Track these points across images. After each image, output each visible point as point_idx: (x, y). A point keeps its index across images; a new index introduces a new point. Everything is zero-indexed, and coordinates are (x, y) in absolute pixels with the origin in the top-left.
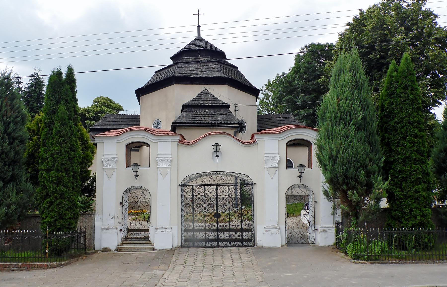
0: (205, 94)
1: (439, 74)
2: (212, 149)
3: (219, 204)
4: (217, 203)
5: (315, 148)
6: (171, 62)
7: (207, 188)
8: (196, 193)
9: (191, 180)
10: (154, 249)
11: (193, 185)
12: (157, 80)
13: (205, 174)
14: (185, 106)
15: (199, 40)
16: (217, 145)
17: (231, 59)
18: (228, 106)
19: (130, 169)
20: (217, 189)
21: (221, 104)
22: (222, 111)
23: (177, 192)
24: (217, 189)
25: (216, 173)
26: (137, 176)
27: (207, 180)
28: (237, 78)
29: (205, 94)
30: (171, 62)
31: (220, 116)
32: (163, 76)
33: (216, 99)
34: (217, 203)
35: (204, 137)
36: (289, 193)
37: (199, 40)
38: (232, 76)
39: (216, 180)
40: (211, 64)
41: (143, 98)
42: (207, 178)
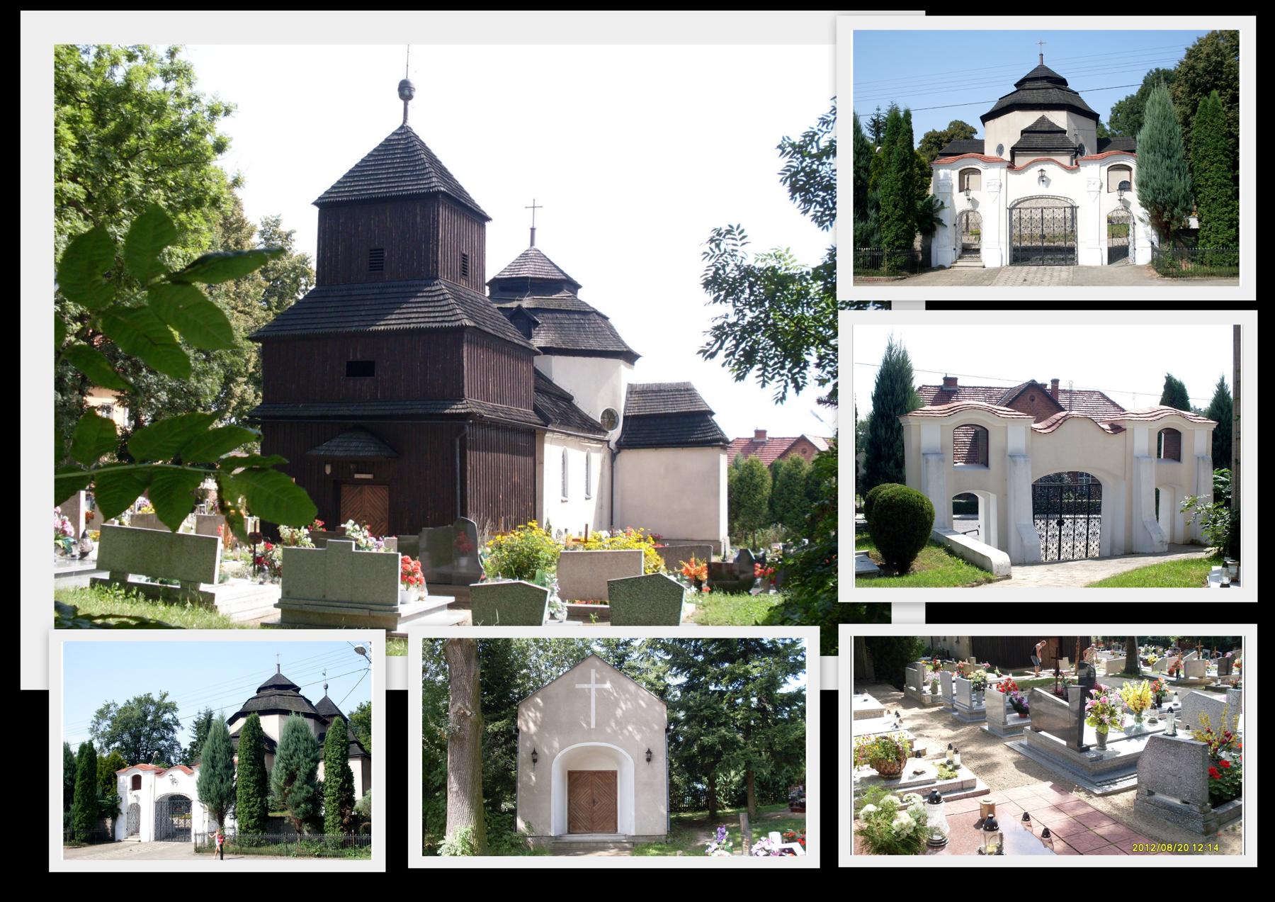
0: (1043, 118)
1: (487, 284)
2: (1038, 175)
3: (1045, 226)
4: (1042, 224)
5: (1134, 172)
6: (1015, 89)
7: (1033, 210)
8: (1023, 216)
9: (1018, 203)
10: (984, 267)
11: (1031, 208)
12: (1000, 107)
13: (1031, 198)
14: (1023, 132)
15: (278, 676)
16: (1042, 170)
17: (1072, 86)
18: (1064, 132)
19: (963, 193)
20: (1042, 211)
21: (1058, 129)
22: (1059, 135)
23: (1004, 215)
24: (1042, 211)
25: (1041, 197)
26: (405, 91)
27: (1033, 203)
28: (1077, 104)
29: (1043, 118)
30: (1015, 89)
31: (1056, 140)
32: (1006, 103)
33: (1053, 124)
34: (1042, 224)
35: (1030, 163)
36: (1110, 215)
37: (278, 676)
38: (1071, 102)
39: (1043, 203)
40: (1051, 90)
41: (987, 123)
42: (1034, 201)
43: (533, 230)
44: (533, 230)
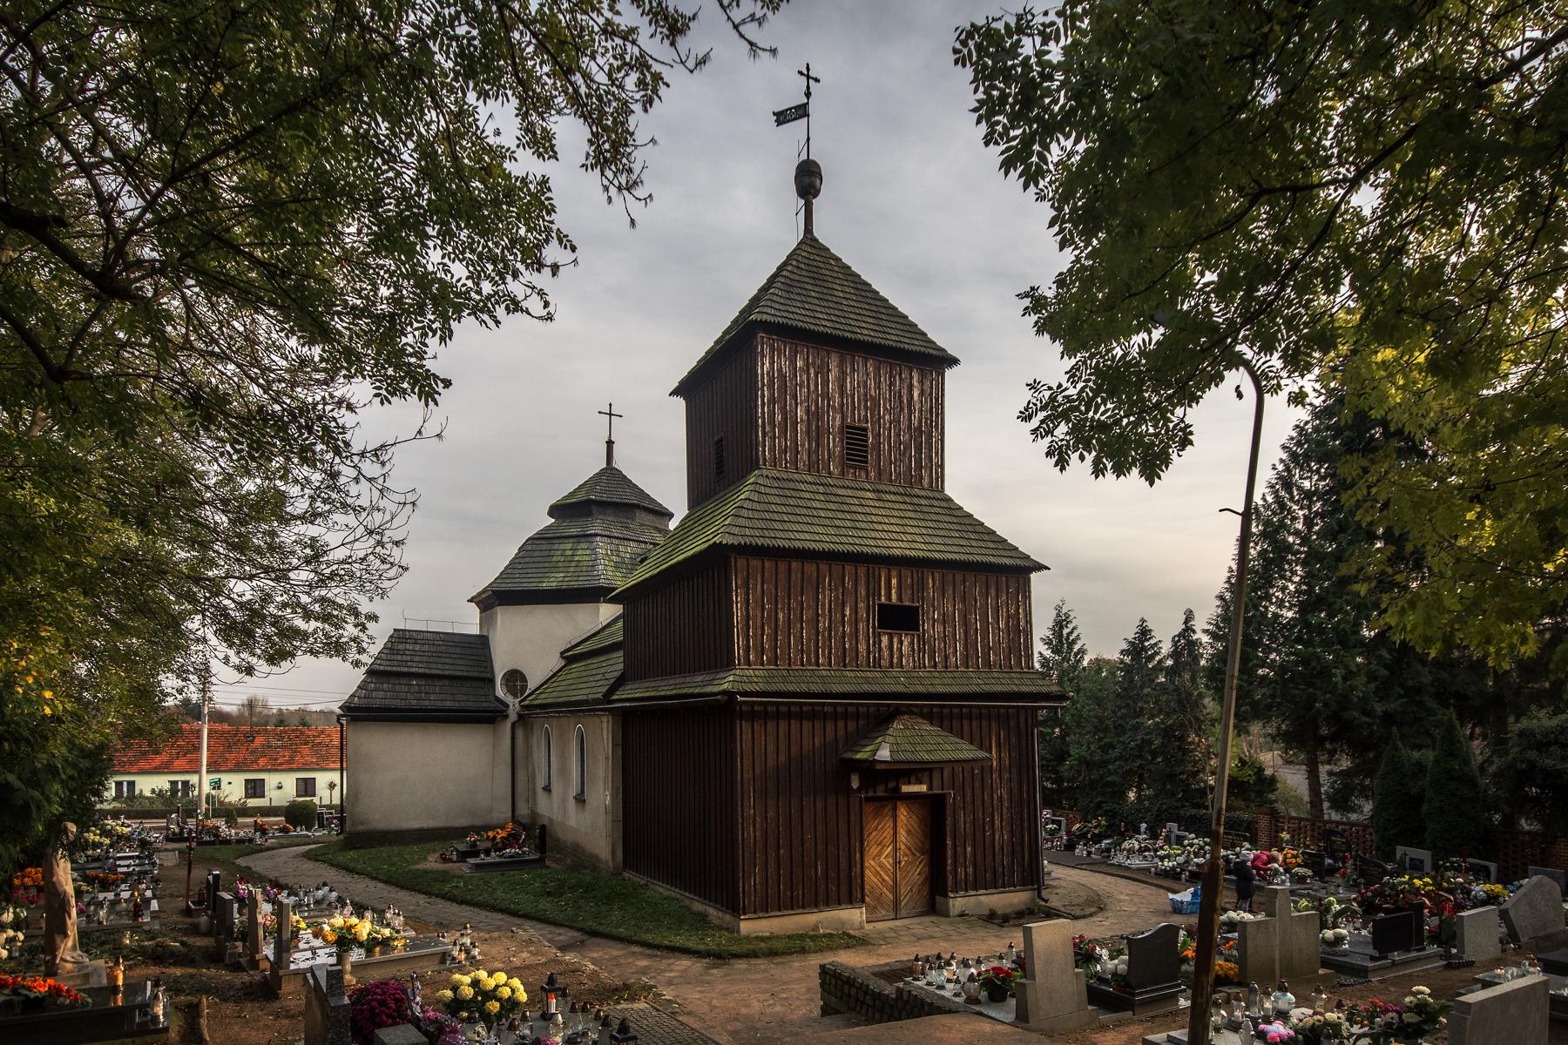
26: (808, 180)
43: (610, 443)
44: (610, 443)
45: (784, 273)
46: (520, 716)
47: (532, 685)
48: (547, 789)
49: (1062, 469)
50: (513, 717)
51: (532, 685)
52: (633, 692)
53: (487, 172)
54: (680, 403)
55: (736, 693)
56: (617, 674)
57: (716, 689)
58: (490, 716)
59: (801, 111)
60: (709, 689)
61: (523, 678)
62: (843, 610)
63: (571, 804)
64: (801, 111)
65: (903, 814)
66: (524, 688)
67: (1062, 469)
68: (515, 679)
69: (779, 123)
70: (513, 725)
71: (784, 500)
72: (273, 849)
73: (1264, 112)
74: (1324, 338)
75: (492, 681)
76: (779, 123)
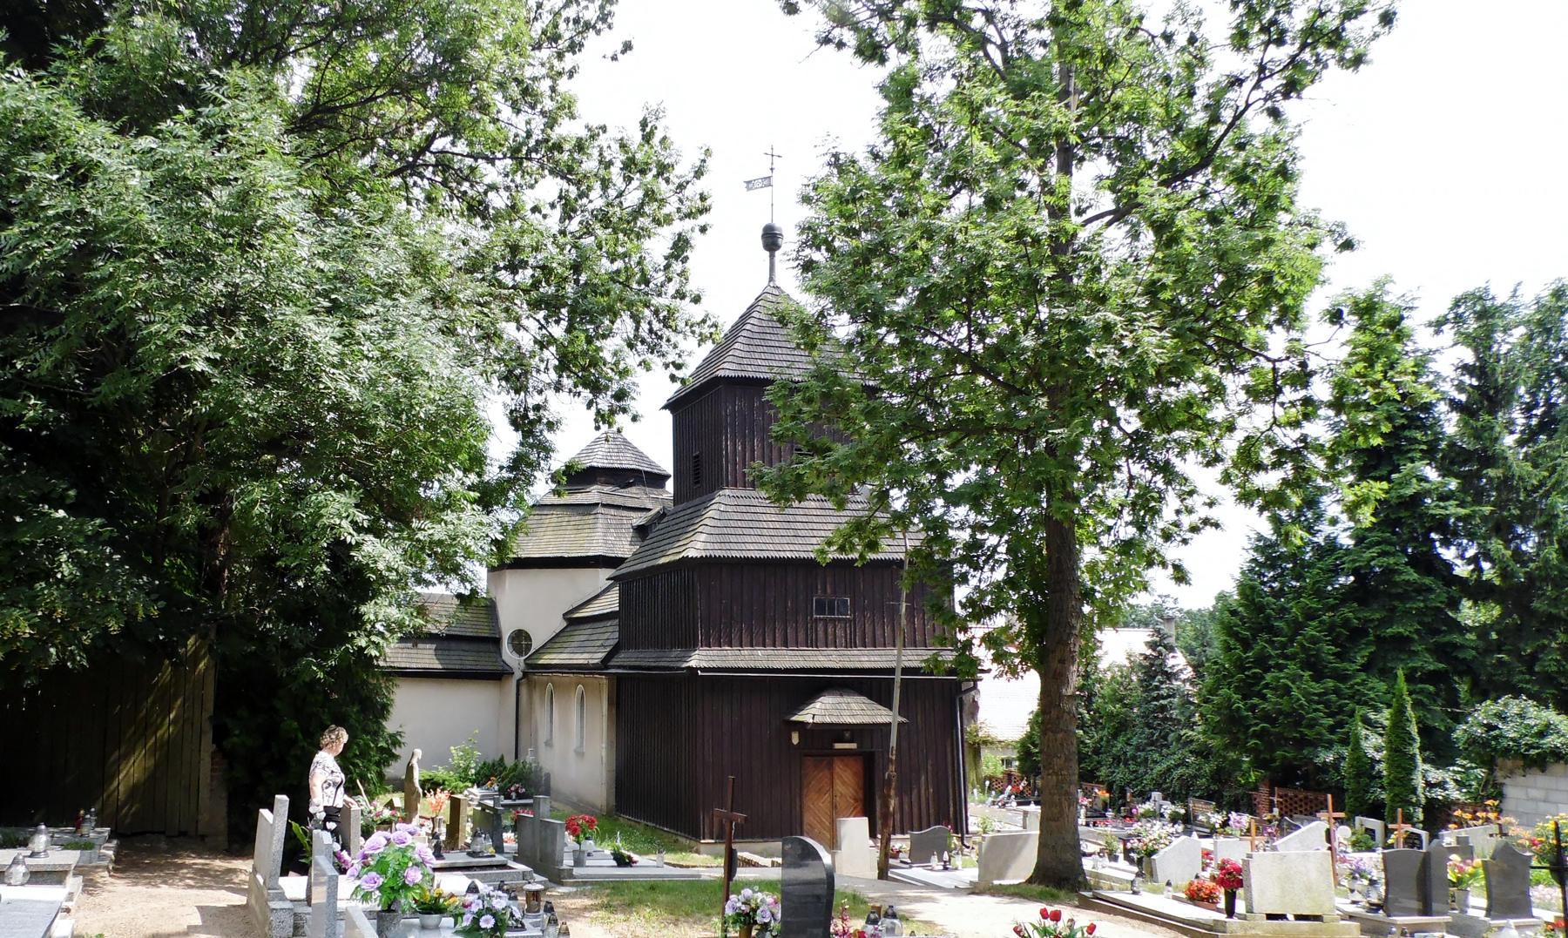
45: (748, 327)
46: (525, 674)
47: (536, 645)
48: (549, 744)
49: (1188, 583)
50: (518, 674)
51: (536, 645)
52: (625, 658)
53: (1062, 661)
54: (668, 417)
55: (697, 669)
56: (613, 642)
57: (685, 665)
58: (498, 675)
59: (767, 181)
60: (678, 665)
61: (528, 638)
62: (786, 603)
63: (572, 755)
64: (767, 181)
65: (839, 767)
66: (529, 647)
67: (1188, 583)
68: (521, 639)
69: (749, 189)
70: (518, 681)
71: (739, 516)
72: (604, 506)
73: (193, 633)
74: (1283, 377)
75: (497, 641)
76: (749, 189)
